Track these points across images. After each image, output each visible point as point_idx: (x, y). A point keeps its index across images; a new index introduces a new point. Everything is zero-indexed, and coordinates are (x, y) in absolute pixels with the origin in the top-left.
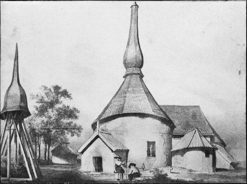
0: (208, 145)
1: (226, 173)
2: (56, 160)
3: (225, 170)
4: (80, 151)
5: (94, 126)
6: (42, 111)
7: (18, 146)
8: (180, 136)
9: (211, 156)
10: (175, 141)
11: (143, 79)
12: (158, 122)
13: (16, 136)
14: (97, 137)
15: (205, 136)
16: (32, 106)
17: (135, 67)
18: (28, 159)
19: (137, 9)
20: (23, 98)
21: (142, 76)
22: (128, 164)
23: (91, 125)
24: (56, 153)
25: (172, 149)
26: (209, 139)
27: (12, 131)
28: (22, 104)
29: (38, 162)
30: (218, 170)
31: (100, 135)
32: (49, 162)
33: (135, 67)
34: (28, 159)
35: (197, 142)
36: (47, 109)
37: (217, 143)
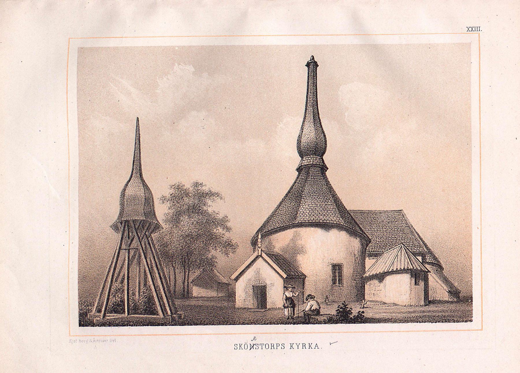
0: (417, 266)
1: (440, 308)
2: (196, 291)
3: (440, 302)
4: (233, 277)
5: (254, 243)
6: (175, 219)
7: (142, 271)
8: (376, 255)
9: (422, 284)
10: (369, 262)
11: (327, 173)
12: (343, 235)
13: (140, 256)
14: (257, 257)
15: (415, 254)
16: (162, 211)
17: (313, 154)
18: (160, 299)
19: (316, 69)
20: (149, 200)
21: (324, 168)
22: (306, 295)
23: (249, 242)
24: (200, 282)
25: (364, 272)
26: (420, 258)
27: (132, 253)
28: (132, 190)
29: (171, 295)
30: (430, 302)
31: (264, 255)
32: (186, 295)
33: (313, 154)
34: (160, 299)
35: (403, 262)
36: (287, 290)
37: (429, 263)
